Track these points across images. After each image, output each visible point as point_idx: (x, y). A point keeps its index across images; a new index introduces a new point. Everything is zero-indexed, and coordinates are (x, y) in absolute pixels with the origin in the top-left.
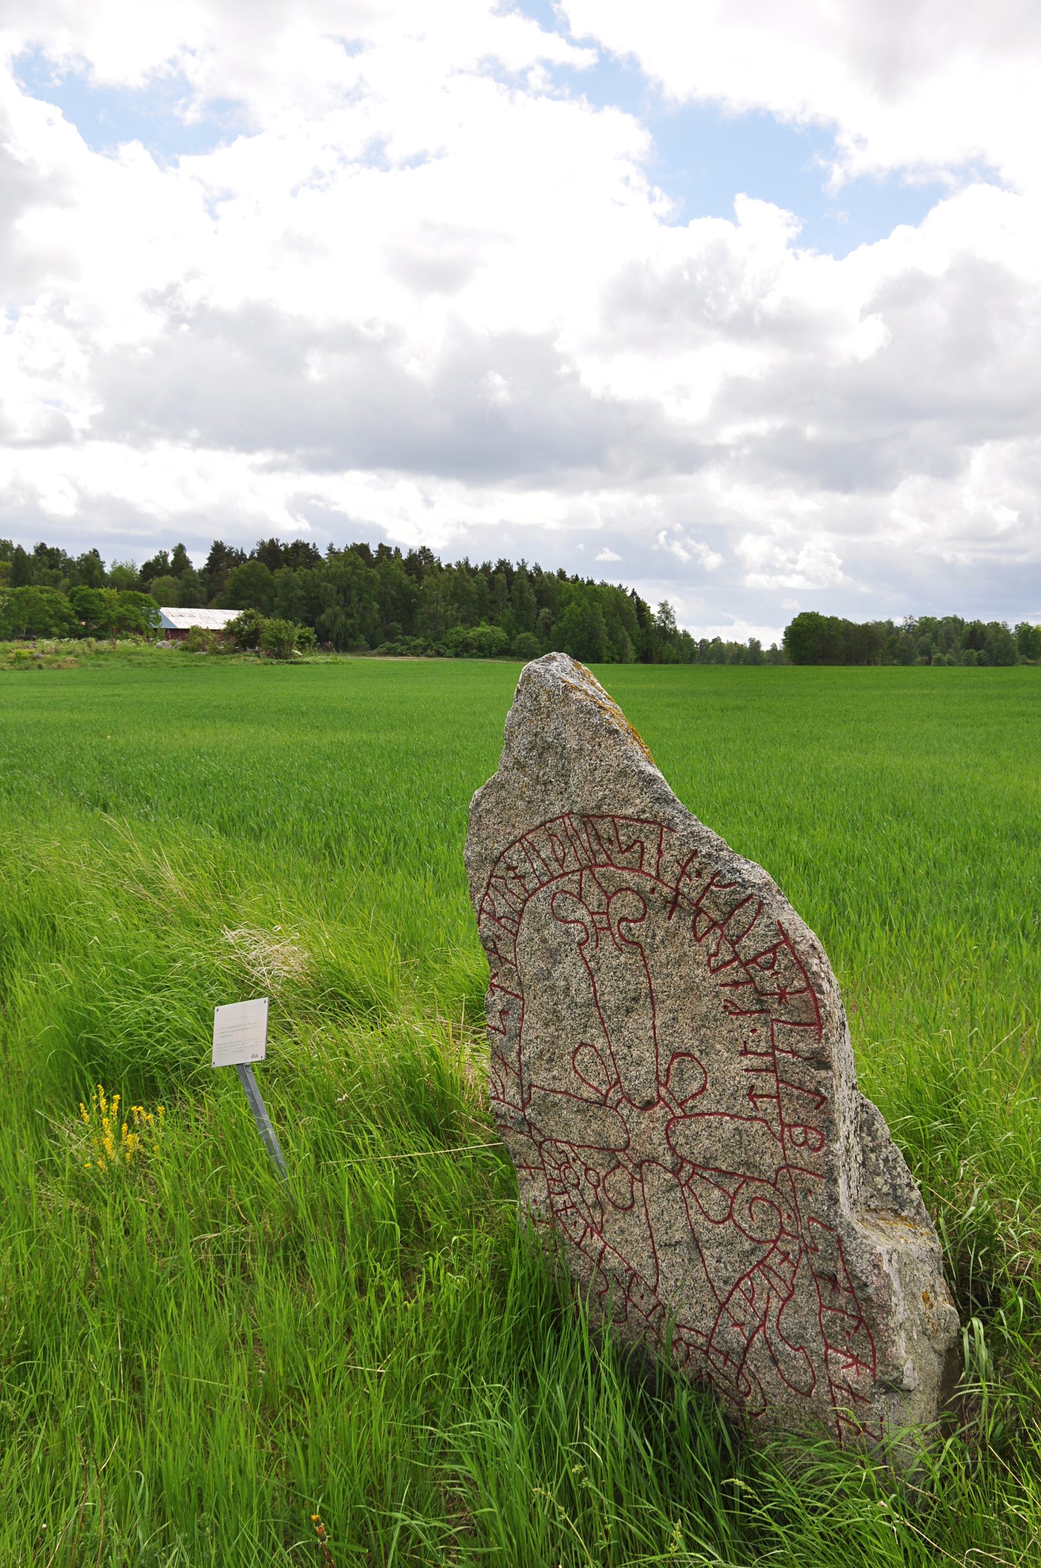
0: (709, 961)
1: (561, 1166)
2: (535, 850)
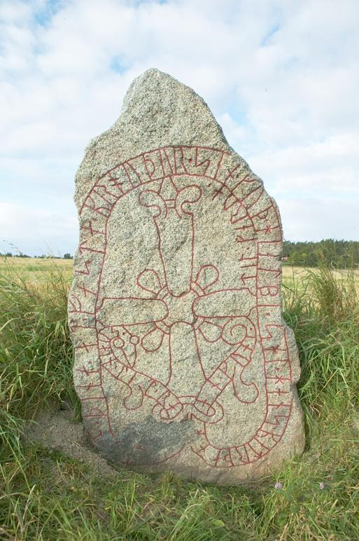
1: (110, 340)
2: (133, 169)
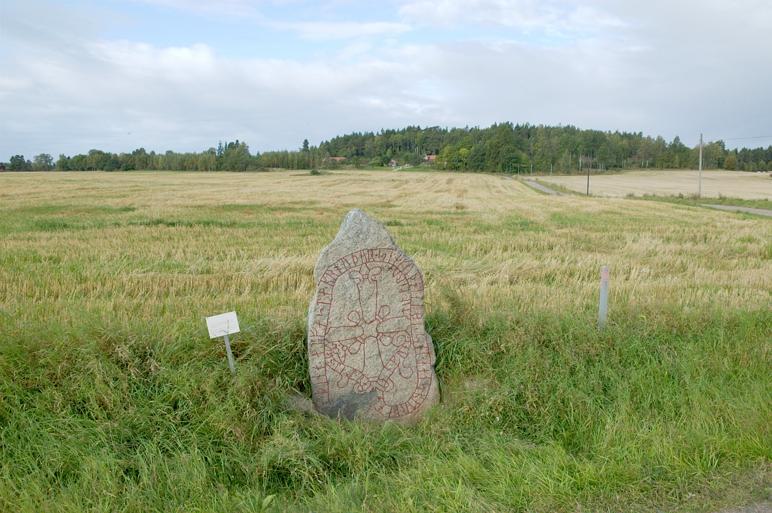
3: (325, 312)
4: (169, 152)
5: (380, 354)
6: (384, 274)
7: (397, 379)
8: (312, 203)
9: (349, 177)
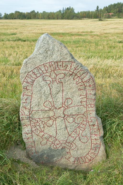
0: (76, 83)
3: (28, 101)
4: (44, 12)
5: (66, 127)
6: (67, 78)
7: (78, 142)
8: (91, 32)
9: (114, 22)
